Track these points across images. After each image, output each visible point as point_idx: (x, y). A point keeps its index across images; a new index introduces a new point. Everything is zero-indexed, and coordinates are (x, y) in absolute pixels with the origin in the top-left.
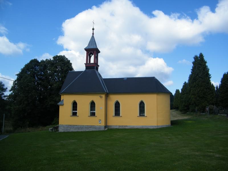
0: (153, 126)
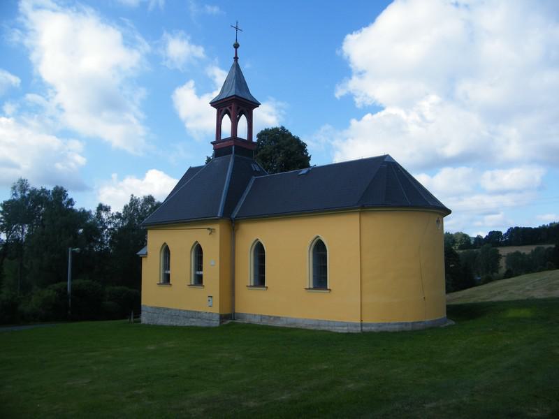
0: (348, 325)
